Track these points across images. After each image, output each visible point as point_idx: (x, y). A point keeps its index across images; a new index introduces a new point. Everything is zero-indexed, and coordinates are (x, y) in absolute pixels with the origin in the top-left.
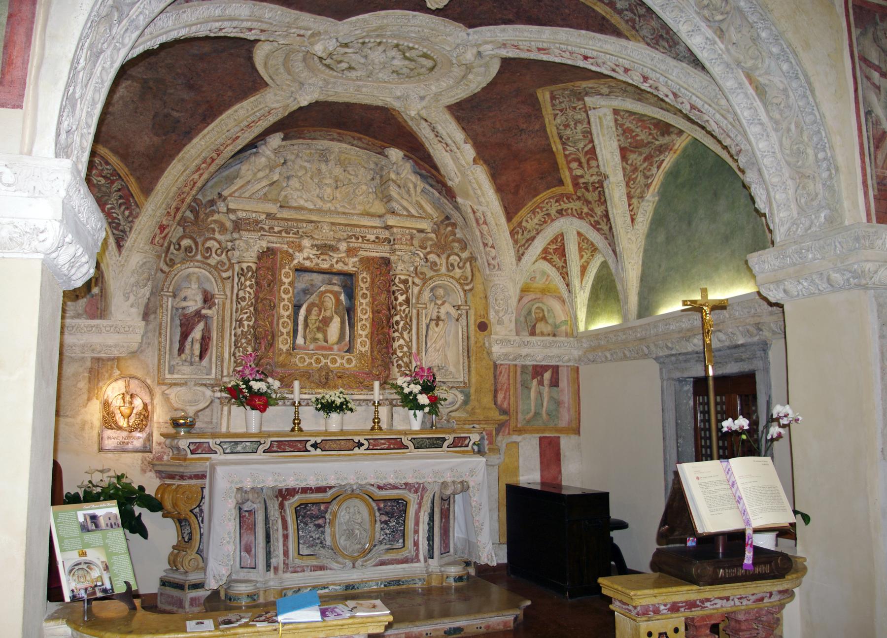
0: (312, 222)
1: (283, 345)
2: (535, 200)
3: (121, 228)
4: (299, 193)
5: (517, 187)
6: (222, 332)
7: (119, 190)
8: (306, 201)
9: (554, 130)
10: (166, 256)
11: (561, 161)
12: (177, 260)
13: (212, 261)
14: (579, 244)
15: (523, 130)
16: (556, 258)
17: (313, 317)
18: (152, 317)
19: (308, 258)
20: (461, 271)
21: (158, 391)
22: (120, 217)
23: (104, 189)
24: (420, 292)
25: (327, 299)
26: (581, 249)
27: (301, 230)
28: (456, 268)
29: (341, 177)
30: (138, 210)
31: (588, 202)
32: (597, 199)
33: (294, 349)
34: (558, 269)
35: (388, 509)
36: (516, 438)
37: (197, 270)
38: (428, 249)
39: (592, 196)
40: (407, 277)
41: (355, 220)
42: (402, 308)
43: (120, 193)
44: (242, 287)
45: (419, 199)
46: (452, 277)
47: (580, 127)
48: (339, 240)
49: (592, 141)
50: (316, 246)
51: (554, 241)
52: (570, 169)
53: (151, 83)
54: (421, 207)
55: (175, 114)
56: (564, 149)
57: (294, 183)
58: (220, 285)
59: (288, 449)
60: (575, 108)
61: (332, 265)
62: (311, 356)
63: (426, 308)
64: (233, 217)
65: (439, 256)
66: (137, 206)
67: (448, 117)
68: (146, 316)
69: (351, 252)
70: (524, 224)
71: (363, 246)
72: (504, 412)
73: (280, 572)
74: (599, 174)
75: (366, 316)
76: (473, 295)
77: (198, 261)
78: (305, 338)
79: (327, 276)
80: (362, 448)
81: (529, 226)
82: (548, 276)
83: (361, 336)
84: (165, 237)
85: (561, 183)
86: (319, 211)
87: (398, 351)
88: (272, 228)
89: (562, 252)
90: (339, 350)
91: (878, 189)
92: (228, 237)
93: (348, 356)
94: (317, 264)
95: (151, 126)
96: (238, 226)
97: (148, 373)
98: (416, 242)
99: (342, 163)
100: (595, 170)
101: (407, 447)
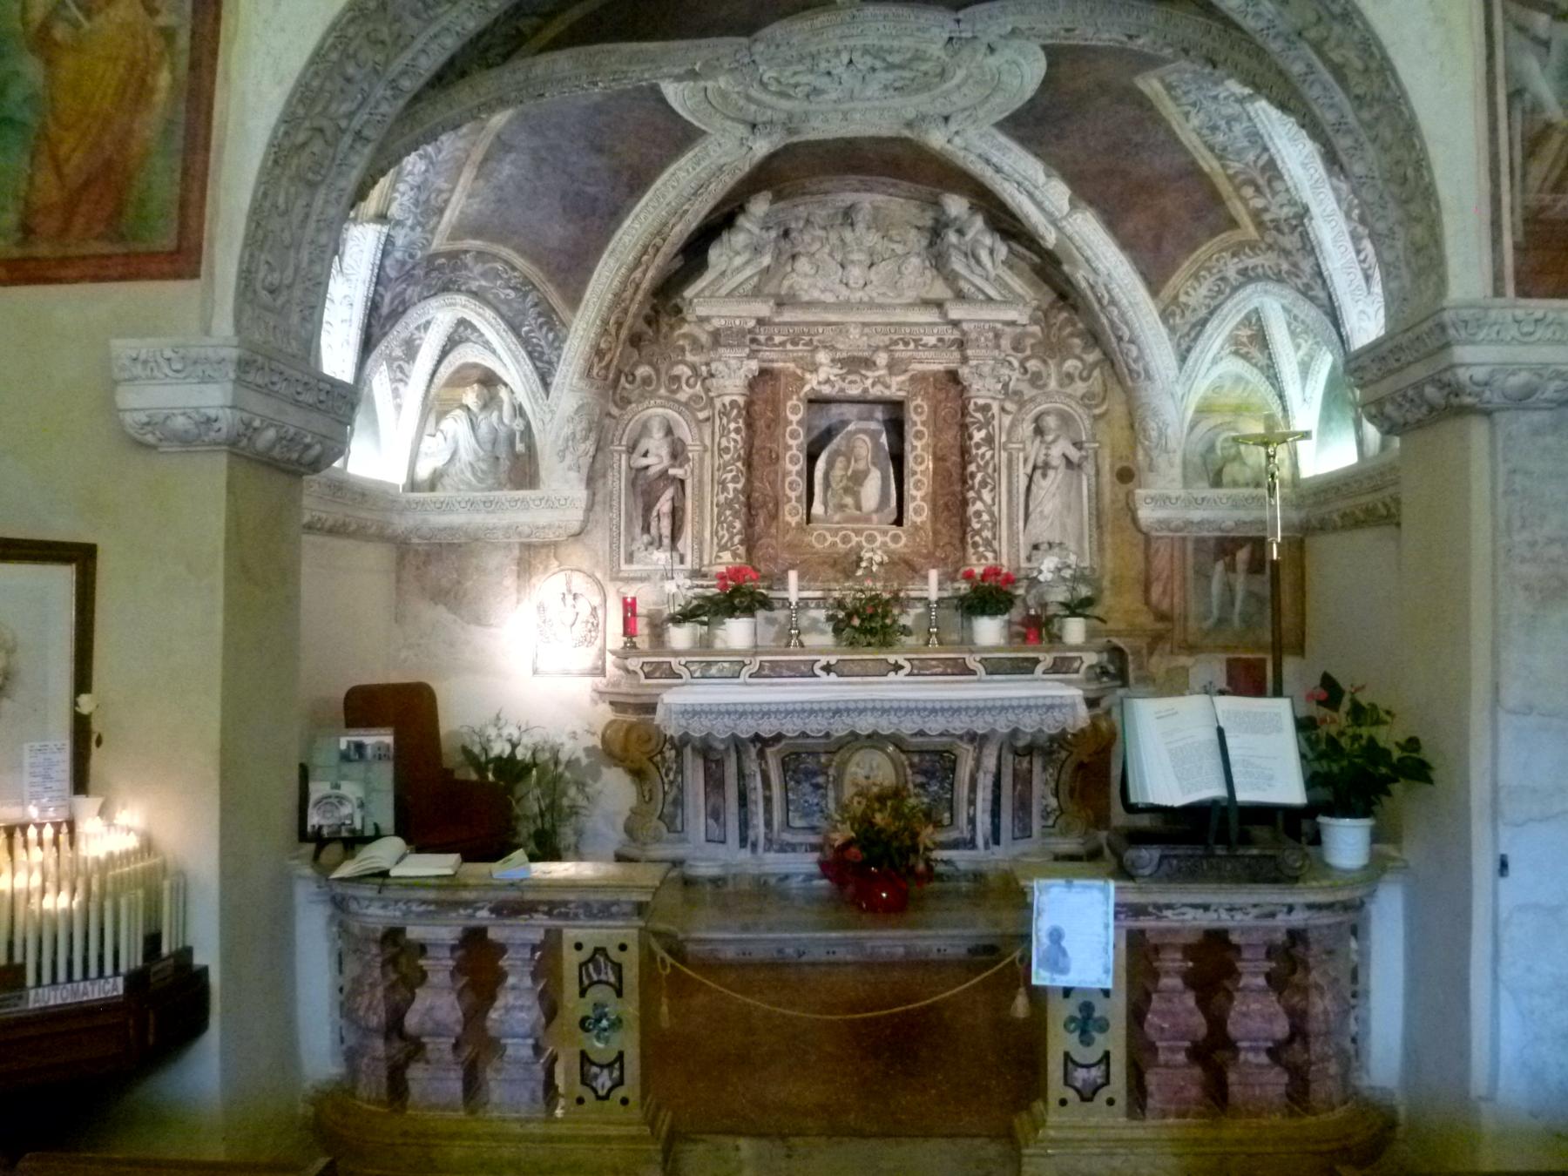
0: (829, 324)
1: (792, 515)
2: (1194, 256)
3: (546, 358)
5: (1158, 240)
6: (700, 499)
7: (536, 305)
8: (823, 291)
9: (1194, 137)
11: (1225, 188)
12: (633, 398)
13: (683, 396)
14: (1289, 325)
15: (1136, 145)
16: (1255, 352)
17: (838, 472)
18: (600, 483)
19: (828, 381)
21: (611, 589)
23: (515, 305)
24: (1013, 425)
25: (859, 443)
26: (1293, 334)
27: (816, 338)
29: (879, 247)
31: (1286, 253)
32: (1299, 245)
33: (809, 521)
34: (1261, 369)
35: (926, 765)
36: (1184, 660)
37: (660, 411)
38: (1028, 352)
39: (1290, 241)
41: (899, 316)
42: (980, 452)
44: (725, 431)
45: (1000, 272)
46: (1070, 396)
47: (1238, 128)
48: (877, 349)
49: (1266, 149)
51: (1247, 321)
52: (1244, 201)
53: (543, 153)
54: (1006, 286)
55: (591, 190)
56: (1224, 167)
57: (803, 264)
58: (695, 430)
59: (785, 673)
60: (1215, 98)
61: (865, 390)
62: (835, 532)
63: (1024, 449)
64: (709, 328)
65: (1045, 362)
67: (1003, 139)
68: (590, 481)
69: (892, 367)
70: (1183, 298)
71: (915, 354)
72: (1162, 617)
73: (760, 850)
74: (1292, 202)
75: (923, 467)
78: (825, 504)
80: (901, 673)
81: (1192, 301)
82: (1248, 383)
83: (914, 498)
84: (607, 367)
85: (1233, 224)
86: (845, 306)
87: (974, 521)
88: (770, 338)
89: (1261, 339)
90: (880, 522)
91: (1526, 233)
93: (894, 530)
94: (842, 390)
97: (597, 564)
98: (1005, 343)
99: (879, 223)
100: (1282, 198)
101: (973, 673)
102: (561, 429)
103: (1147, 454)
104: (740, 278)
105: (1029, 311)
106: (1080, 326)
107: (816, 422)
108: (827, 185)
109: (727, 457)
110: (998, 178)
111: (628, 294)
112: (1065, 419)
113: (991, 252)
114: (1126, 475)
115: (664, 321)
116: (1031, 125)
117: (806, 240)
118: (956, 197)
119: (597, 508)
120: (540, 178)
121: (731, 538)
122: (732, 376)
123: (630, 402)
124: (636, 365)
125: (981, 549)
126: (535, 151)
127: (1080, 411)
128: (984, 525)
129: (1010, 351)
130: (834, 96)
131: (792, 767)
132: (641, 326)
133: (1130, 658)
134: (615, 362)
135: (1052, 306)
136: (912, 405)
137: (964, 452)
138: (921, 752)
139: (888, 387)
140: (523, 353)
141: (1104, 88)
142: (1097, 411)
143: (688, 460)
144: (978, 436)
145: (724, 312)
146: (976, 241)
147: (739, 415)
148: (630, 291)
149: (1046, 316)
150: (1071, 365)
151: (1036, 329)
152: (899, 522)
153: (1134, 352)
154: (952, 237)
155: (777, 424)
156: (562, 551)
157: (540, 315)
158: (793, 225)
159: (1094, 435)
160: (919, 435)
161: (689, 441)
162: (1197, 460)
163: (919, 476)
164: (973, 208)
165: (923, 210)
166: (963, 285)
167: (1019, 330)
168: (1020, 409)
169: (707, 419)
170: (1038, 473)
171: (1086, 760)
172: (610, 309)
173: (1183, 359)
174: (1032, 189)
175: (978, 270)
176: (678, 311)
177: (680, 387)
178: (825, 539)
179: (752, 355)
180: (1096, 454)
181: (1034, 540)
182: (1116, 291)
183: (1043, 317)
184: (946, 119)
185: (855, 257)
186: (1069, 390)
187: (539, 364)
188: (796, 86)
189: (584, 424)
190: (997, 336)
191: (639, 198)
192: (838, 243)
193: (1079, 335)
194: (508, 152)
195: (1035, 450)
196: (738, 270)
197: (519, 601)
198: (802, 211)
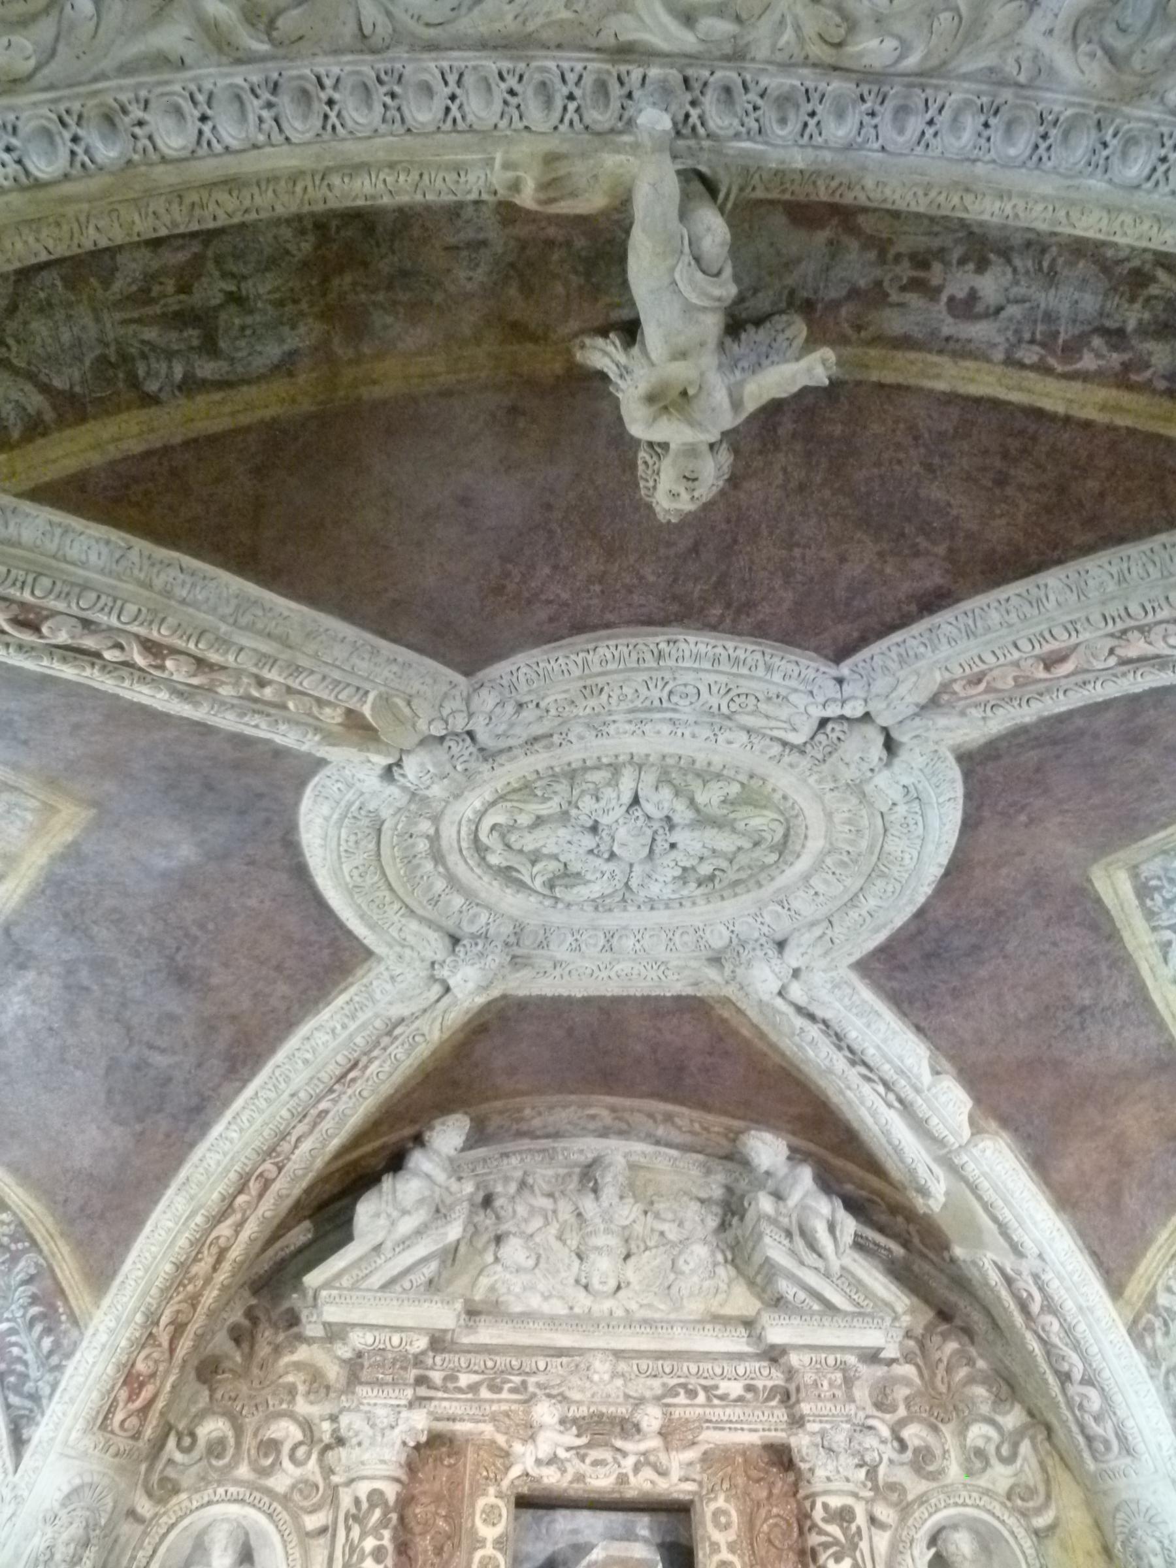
0: (560, 1352)
3: (29, 1387)
4: (525, 1278)
5: (1115, 1191)
7: (30, 1280)
8: (546, 1298)
10: (150, 1469)
12: (186, 1481)
13: (280, 1482)
15: (1082, 1010)
19: (553, 1460)
20: (1008, 1470)
22: (29, 1356)
24: (895, 1549)
27: (532, 1380)
28: (994, 1461)
29: (638, 1228)
30: (75, 1333)
37: (234, 1510)
38: (902, 1412)
40: (849, 1501)
41: (680, 1341)
43: (32, 1289)
46: (986, 1492)
48: (640, 1401)
50: (574, 1421)
54: (859, 1285)
57: (514, 1251)
58: (297, 1553)
61: (622, 1479)
65: (935, 1429)
66: (75, 1322)
67: (866, 994)
70: (1163, 1299)
76: (1064, 1547)
77: (238, 1482)
79: (618, 1517)
88: (451, 1378)
92: (327, 1408)
94: (580, 1478)
95: (102, 1097)
96: (355, 1370)
98: (862, 1393)
99: (637, 1186)
106: (981, 1364)
107: (528, 1548)
108: (561, 1117)
110: (854, 1074)
111: (201, 1268)
113: (832, 1228)
115: (266, 1335)
116: (914, 968)
117: (519, 1212)
118: (768, 1136)
120: (74, 1025)
122: (378, 1440)
123: (176, 1491)
124: (201, 1416)
126: (70, 969)
127: (1011, 1521)
129: (871, 1410)
130: (596, 889)
132: (221, 1342)
134: (160, 1404)
135: (929, 1329)
136: (709, 1509)
139: (663, 1473)
141: (1038, 886)
142: (1040, 1522)
145: (373, 1318)
146: (803, 1207)
147: (384, 1523)
148: (208, 1260)
149: (922, 1346)
150: (978, 1433)
151: (909, 1370)
153: (1095, 1402)
154: (765, 1204)
155: (457, 1547)
157: (34, 1300)
158: (499, 1189)
164: (796, 1155)
165: (708, 1172)
166: (784, 1286)
169: (323, 1530)
172: (166, 1294)
174: (909, 1094)
175: (811, 1258)
176: (293, 1320)
177: (277, 1462)
179: (417, 1402)
182: (1054, 1286)
183: (919, 1348)
184: (781, 945)
185: (600, 1240)
186: (983, 1482)
187: (14, 1400)
188: (535, 858)
189: (76, 1530)
190: (848, 1382)
191: (245, 1082)
192: (572, 1219)
193: (986, 1381)
194: (22, 967)
196: (405, 1243)
198: (514, 1166)
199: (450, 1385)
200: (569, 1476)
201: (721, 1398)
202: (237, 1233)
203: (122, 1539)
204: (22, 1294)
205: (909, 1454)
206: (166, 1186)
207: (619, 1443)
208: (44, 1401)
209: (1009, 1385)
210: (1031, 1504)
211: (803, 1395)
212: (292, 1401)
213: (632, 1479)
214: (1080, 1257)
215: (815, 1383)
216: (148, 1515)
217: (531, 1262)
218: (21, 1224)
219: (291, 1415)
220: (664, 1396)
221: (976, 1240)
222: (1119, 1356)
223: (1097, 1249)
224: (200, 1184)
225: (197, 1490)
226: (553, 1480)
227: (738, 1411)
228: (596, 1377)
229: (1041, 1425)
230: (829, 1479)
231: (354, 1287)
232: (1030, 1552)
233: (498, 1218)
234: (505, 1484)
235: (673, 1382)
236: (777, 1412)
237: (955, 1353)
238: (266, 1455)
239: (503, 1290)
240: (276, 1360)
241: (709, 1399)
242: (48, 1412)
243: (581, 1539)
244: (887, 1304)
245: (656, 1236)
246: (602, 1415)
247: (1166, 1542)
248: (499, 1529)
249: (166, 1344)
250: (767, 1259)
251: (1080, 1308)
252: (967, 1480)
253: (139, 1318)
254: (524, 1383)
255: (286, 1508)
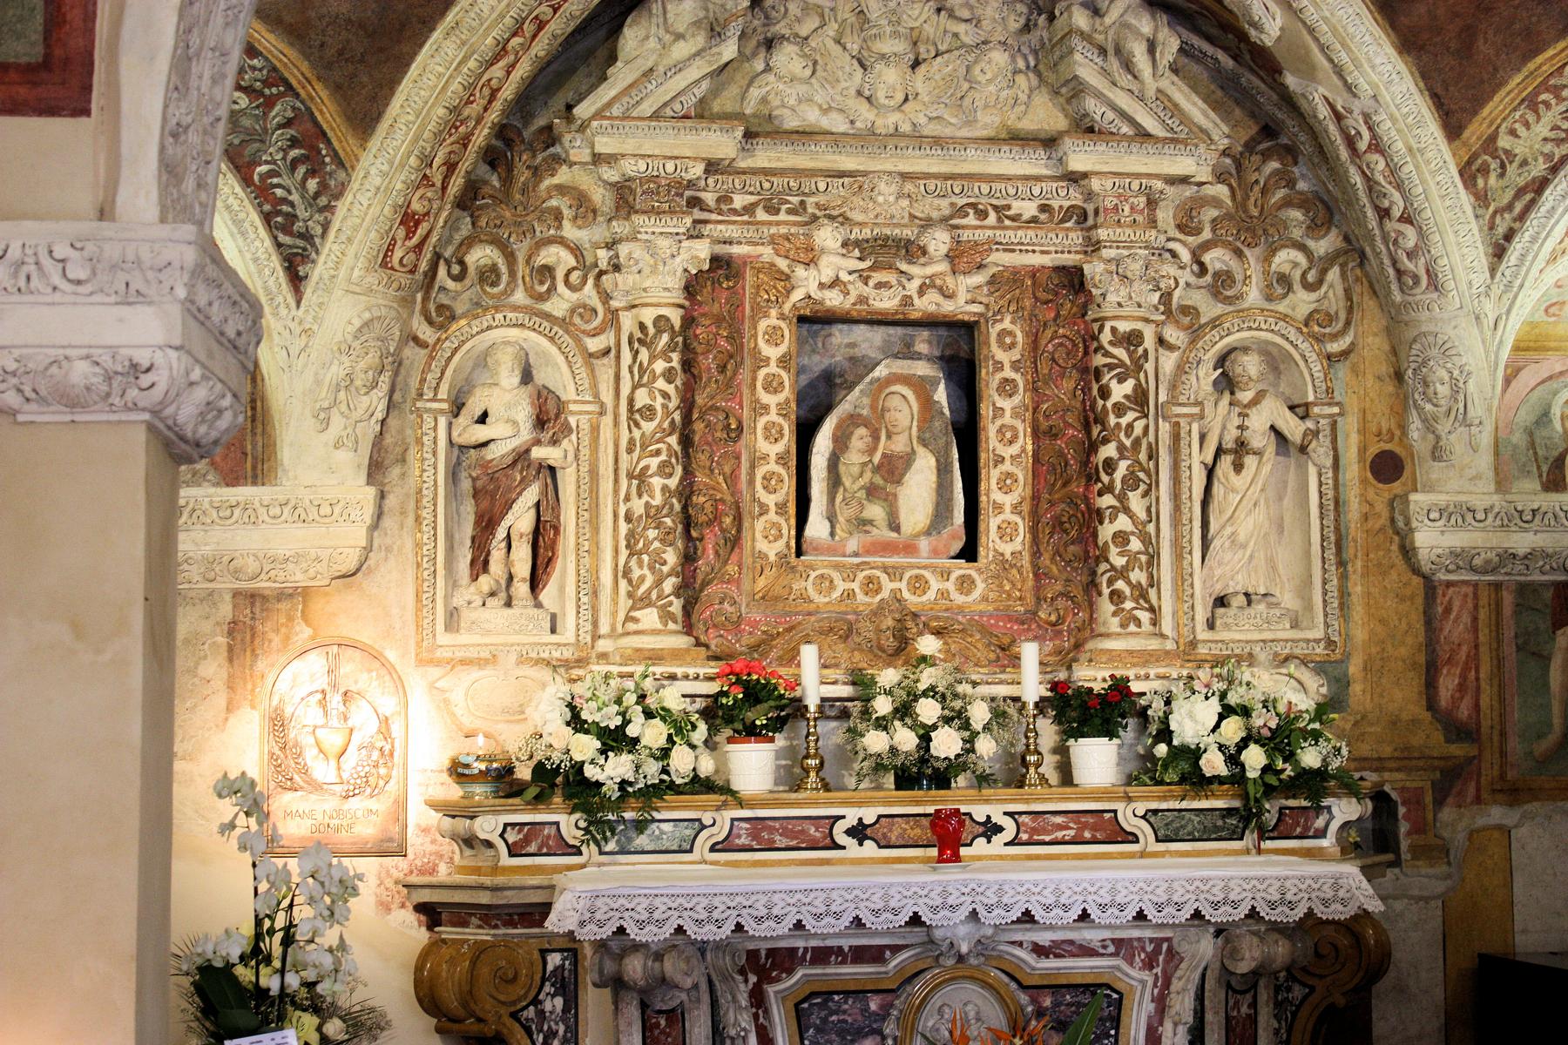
0: (842, 174)
1: (767, 537)
2: (1531, 66)
3: (298, 226)
4: (802, 89)
5: (1468, 37)
7: (288, 123)
8: (825, 111)
10: (425, 299)
17: (854, 458)
19: (836, 283)
22: (295, 197)
24: (1181, 369)
25: (895, 402)
27: (811, 200)
28: (1297, 286)
29: (929, 30)
30: (341, 175)
36: (1497, 814)
37: (514, 333)
38: (1207, 234)
40: (1139, 325)
44: (642, 377)
45: (1164, 84)
46: (1284, 318)
48: (927, 224)
50: (857, 243)
54: (1175, 109)
57: (787, 58)
58: (583, 373)
59: (780, 841)
61: (907, 301)
63: (1202, 417)
64: (611, 175)
65: (1239, 253)
66: (341, 164)
68: (375, 469)
69: (961, 258)
70: (1504, 142)
72: (1458, 731)
75: (1014, 449)
76: (1355, 370)
77: (515, 308)
78: (832, 518)
80: (999, 839)
81: (1520, 149)
83: (999, 508)
86: (867, 138)
87: (1114, 551)
88: (725, 199)
90: (935, 553)
92: (599, 232)
93: (962, 568)
94: (862, 300)
96: (625, 198)
98: (1165, 215)
102: (326, 366)
103: (1429, 424)
104: (679, 82)
105: (1212, 157)
109: (648, 427)
111: (473, 110)
112: (1275, 361)
113: (1152, 48)
114: (1387, 467)
119: (387, 522)
121: (658, 583)
122: (657, 268)
123: (453, 318)
124: (468, 243)
125: (1128, 605)
127: (1304, 346)
128: (1133, 558)
131: (815, 1019)
133: (1402, 810)
134: (434, 239)
135: (1250, 146)
136: (994, 331)
137: (1091, 418)
138: (1056, 988)
140: (255, 217)
142: (1334, 347)
143: (567, 429)
144: (1120, 391)
147: (671, 347)
149: (1239, 166)
150: (1286, 259)
151: (1222, 191)
152: (969, 552)
153: (1410, 237)
156: (318, 606)
157: (294, 142)
159: (1329, 391)
160: (1007, 388)
161: (568, 393)
162: (1518, 438)
163: (1007, 466)
166: (1091, 105)
167: (1189, 191)
168: (1193, 342)
169: (607, 352)
170: (1226, 462)
171: (1341, 1001)
173: (1499, 253)
175: (1125, 80)
178: (832, 586)
180: (1334, 425)
181: (1218, 589)
182: (1385, 128)
183: (1234, 169)
186: (1282, 307)
187: (282, 238)
189: (372, 358)
190: (1152, 203)
192: (853, 19)
193: (1304, 203)
195: (1220, 419)
196: (678, 67)
197: (230, 708)
199: (724, 207)
200: (852, 298)
201: (1012, 219)
202: (509, 73)
203: (406, 363)
204: (279, 138)
205: (1208, 278)
206: (432, 29)
207: (904, 267)
208: (317, 241)
209: (1326, 210)
210: (1327, 330)
211: (1101, 219)
212: (560, 227)
213: (916, 301)
214: (1417, 97)
215: (1116, 208)
216: (431, 341)
217: (808, 72)
218: (274, 69)
219: (562, 241)
220: (952, 217)
221: (1309, 71)
222: (1442, 197)
223: (1439, 91)
224: (471, 29)
225: (476, 317)
226: (836, 303)
227: (1031, 233)
228: (881, 199)
229: (1354, 252)
230: (1120, 305)
231: (625, 117)
232: (1319, 375)
233: (767, 17)
234: (787, 307)
235: (961, 202)
236: (1072, 235)
237: (1276, 172)
238: (542, 283)
239: (776, 103)
240: (536, 185)
241: (1000, 220)
242: (325, 251)
243: (858, 352)
244: (1202, 130)
245: (948, 38)
246: (887, 238)
247: (1456, 373)
248: (783, 349)
249: (439, 184)
250: (1076, 77)
251: (1410, 150)
252: (1267, 305)
253: (413, 161)
254: (802, 203)
255: (567, 332)
